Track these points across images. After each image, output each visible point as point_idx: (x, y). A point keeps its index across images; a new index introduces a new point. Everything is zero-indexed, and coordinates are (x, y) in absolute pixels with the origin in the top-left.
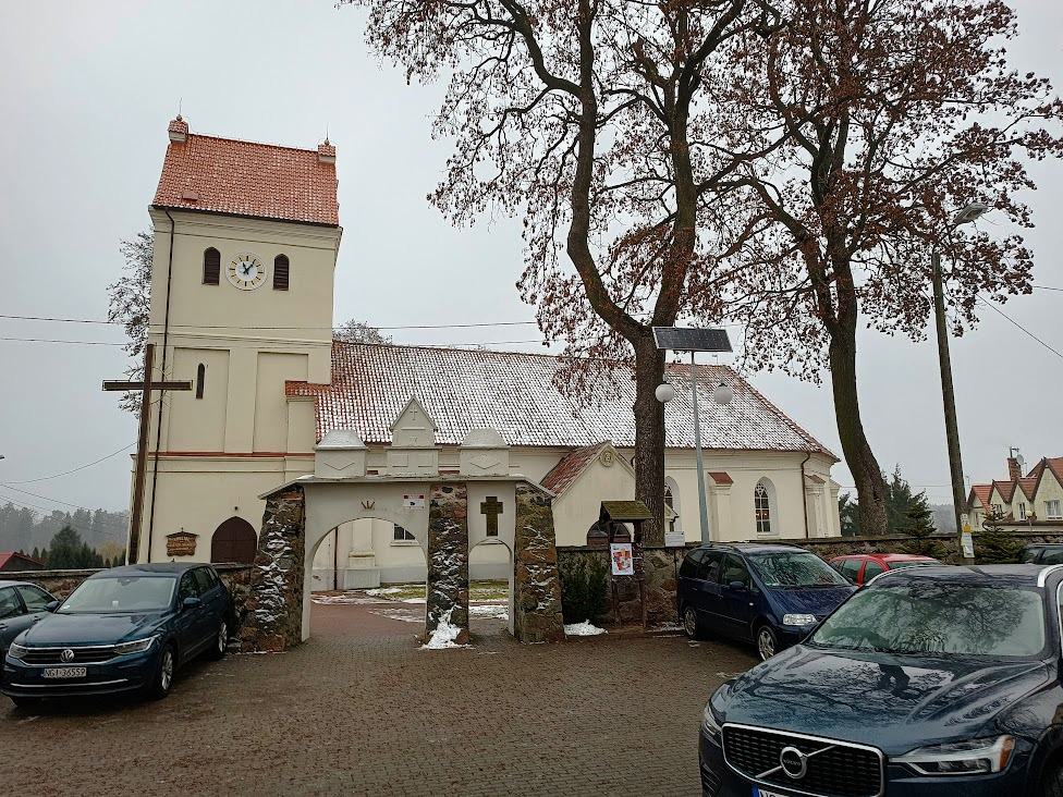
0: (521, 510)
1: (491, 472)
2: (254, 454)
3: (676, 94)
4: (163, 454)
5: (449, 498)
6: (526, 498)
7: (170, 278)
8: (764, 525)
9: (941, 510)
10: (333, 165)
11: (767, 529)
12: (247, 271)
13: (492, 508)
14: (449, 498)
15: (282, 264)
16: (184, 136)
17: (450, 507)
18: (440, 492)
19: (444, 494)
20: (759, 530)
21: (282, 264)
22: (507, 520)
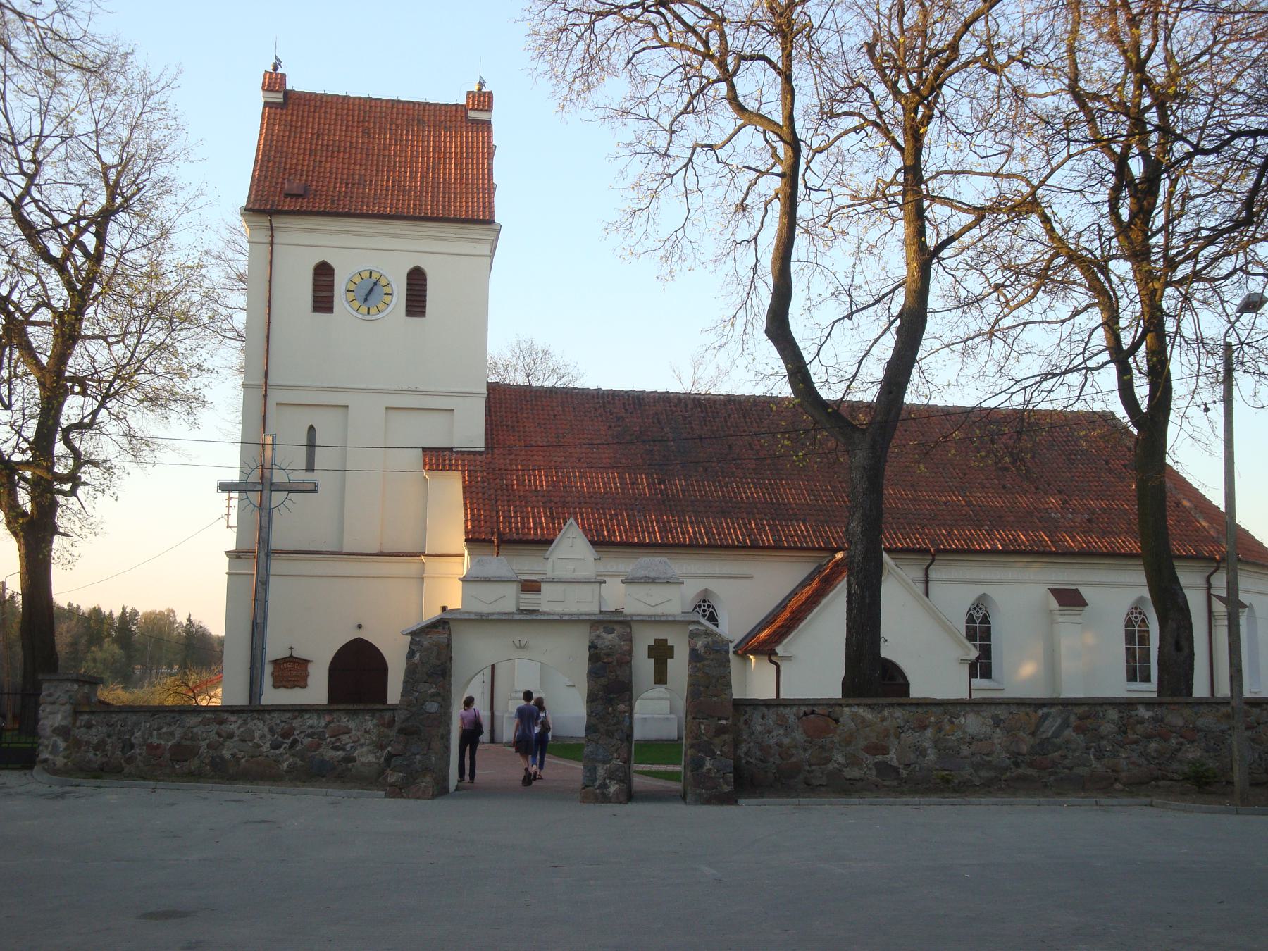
0: (695, 656)
3: (1099, 275)
5: (609, 639)
6: (700, 644)
8: (981, 668)
10: (488, 124)
11: (987, 673)
13: (661, 652)
15: (417, 280)
16: (281, 95)
17: (611, 651)
19: (604, 634)
21: (417, 280)
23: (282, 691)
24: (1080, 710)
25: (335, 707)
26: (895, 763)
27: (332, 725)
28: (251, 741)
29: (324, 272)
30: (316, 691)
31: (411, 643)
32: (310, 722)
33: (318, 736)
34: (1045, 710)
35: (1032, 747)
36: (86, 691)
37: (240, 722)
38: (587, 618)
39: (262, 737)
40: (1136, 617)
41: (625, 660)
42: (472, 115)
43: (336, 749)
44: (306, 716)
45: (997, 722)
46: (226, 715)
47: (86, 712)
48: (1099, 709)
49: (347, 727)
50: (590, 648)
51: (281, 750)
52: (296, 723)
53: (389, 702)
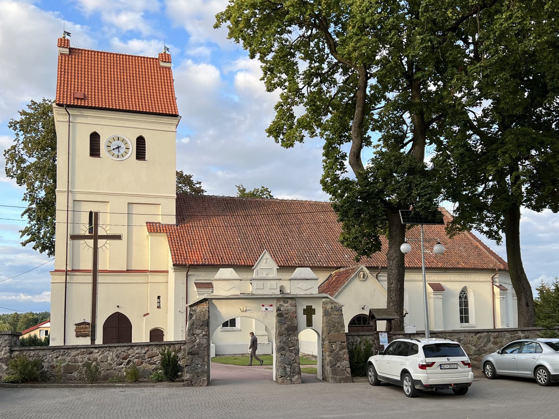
0: (326, 313)
1: (308, 292)
2: (128, 271)
4: (69, 271)
5: (286, 306)
6: (329, 306)
7: (311, 279)
8: (464, 317)
9: (309, 358)
12: (118, 147)
13: (309, 312)
14: (286, 306)
15: (141, 141)
16: (68, 50)
18: (281, 303)
20: (462, 321)
21: (141, 141)
22: (318, 318)
23: (81, 338)
25: (106, 345)
27: (149, 352)
29: (95, 138)
32: (137, 351)
33: (141, 357)
34: (479, 335)
35: (475, 351)
36: (15, 340)
37: (100, 352)
38: (276, 296)
40: (463, 295)
41: (295, 316)
42: (162, 64)
43: (152, 364)
44: (135, 348)
46: (92, 350)
47: (16, 350)
48: (502, 333)
50: (277, 311)
51: (122, 366)
52: (130, 352)
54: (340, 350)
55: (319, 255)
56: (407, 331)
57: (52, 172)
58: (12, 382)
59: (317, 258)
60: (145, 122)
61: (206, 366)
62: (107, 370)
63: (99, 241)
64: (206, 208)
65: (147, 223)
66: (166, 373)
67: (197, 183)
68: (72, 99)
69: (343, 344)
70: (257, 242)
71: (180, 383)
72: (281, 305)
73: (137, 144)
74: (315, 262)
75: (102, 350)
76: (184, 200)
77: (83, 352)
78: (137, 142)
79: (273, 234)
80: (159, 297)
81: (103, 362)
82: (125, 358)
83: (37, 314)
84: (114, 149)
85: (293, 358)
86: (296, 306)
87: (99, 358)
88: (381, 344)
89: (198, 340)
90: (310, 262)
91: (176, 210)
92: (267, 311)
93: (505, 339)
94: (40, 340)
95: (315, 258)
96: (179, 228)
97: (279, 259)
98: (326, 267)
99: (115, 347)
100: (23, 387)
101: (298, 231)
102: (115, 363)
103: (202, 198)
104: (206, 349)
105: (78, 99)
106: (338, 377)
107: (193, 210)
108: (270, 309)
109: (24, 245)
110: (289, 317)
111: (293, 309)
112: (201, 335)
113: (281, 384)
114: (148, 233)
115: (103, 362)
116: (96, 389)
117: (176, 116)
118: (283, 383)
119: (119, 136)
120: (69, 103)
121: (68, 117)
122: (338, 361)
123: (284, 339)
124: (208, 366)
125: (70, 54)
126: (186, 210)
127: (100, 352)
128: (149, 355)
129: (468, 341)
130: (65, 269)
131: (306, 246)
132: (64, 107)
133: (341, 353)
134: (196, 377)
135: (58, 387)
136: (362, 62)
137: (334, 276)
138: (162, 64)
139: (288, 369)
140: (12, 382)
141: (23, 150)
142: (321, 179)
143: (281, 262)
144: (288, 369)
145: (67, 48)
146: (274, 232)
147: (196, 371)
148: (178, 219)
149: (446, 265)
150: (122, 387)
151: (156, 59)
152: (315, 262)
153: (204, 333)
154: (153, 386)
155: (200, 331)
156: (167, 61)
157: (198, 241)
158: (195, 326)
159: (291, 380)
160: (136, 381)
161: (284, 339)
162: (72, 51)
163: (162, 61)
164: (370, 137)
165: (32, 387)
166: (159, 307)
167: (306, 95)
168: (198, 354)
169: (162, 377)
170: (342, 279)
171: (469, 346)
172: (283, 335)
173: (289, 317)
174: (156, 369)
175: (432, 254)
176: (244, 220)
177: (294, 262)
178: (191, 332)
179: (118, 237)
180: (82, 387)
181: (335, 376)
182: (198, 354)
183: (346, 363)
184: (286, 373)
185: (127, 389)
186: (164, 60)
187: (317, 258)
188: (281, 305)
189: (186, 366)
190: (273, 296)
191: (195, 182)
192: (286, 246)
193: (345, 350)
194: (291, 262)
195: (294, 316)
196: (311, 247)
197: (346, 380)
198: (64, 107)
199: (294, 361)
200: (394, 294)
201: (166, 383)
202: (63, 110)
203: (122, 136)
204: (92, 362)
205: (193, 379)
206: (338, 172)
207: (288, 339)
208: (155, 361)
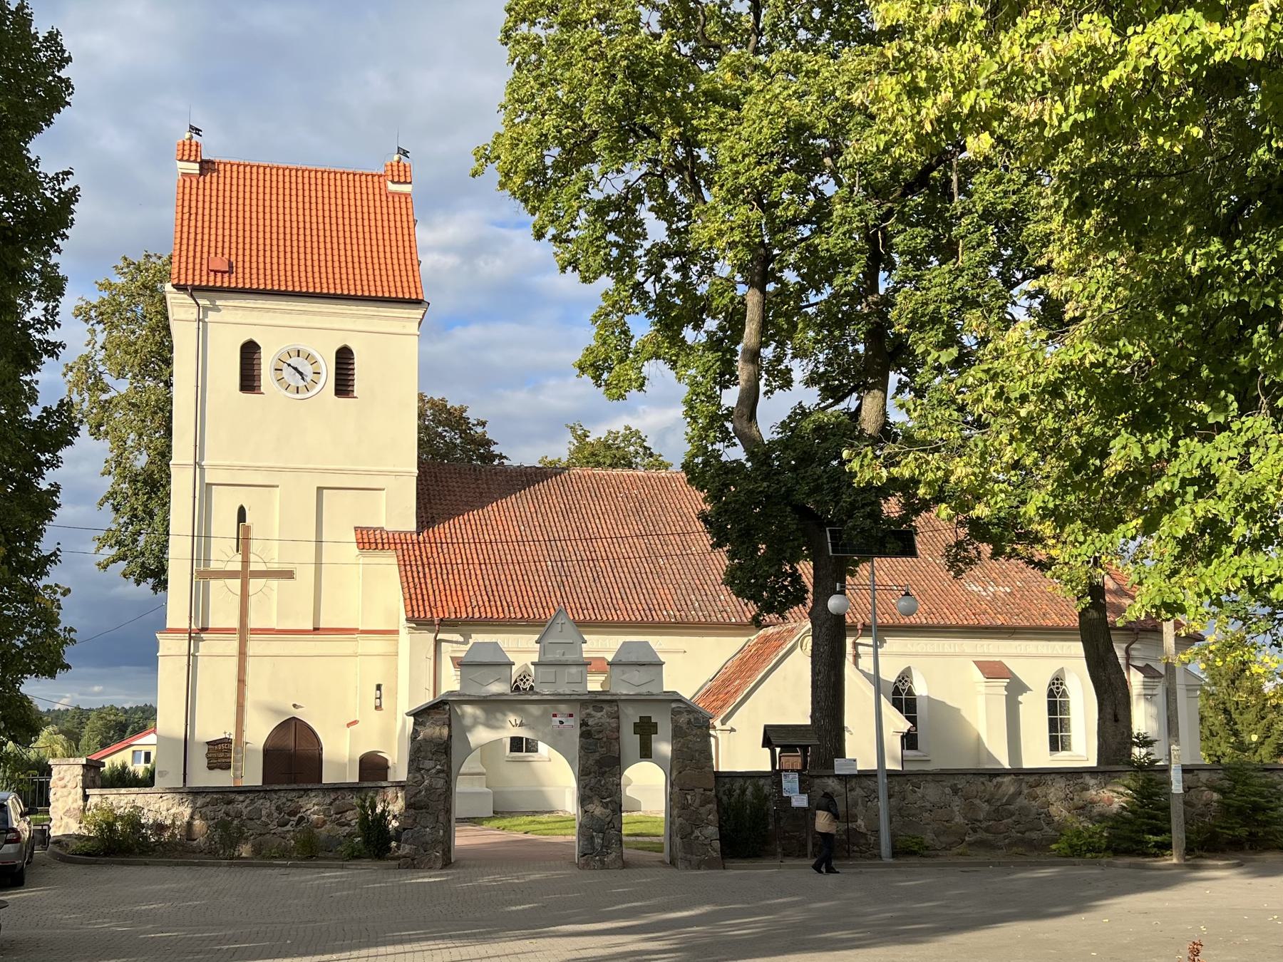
1: (644, 690)
5: (598, 717)
6: (683, 719)
15: (344, 357)
16: (197, 166)
18: (590, 710)
21: (344, 357)
23: (217, 772)
24: (1031, 779)
25: (366, 784)
26: (863, 830)
27: (337, 802)
28: (259, 819)
29: (250, 351)
30: (253, 775)
31: (415, 724)
35: (988, 813)
37: (248, 801)
39: (269, 816)
40: (1058, 688)
42: (392, 187)
45: (955, 791)
46: (232, 796)
49: (352, 804)
50: (581, 725)
51: (288, 827)
53: (324, 781)
54: (702, 806)
55: (722, 597)
56: (841, 770)
57: (163, 411)
58: (87, 854)
59: (719, 603)
60: (353, 316)
61: (441, 832)
62: (260, 835)
63: (252, 581)
64: (481, 493)
65: (356, 529)
66: (367, 842)
67: (478, 424)
68: (204, 273)
69: (708, 793)
70: (588, 568)
71: (393, 863)
72: (589, 715)
73: (337, 363)
74: (713, 614)
75: (251, 796)
76: (436, 477)
77: (217, 799)
78: (337, 358)
79: (624, 551)
80: (379, 687)
81: (252, 819)
82: (291, 814)
83: (126, 711)
84: (289, 365)
85: (608, 819)
86: (618, 718)
87: (245, 812)
88: (785, 795)
89: (426, 782)
90: (700, 614)
91: (417, 494)
92: (561, 726)
93: (1053, 789)
94: (134, 774)
95: (713, 603)
96: (421, 537)
97: (634, 606)
98: (736, 624)
99: (276, 791)
100: (106, 863)
101: (680, 543)
102: (275, 823)
103: (475, 470)
104: (442, 797)
105: (216, 272)
106: (695, 857)
107: (454, 498)
108: (569, 722)
109: (105, 568)
110: (605, 739)
111: (613, 722)
112: (434, 771)
113: (583, 868)
114: (357, 552)
115: (252, 819)
116: (237, 869)
117: (418, 302)
118: (586, 866)
119: (299, 347)
120: (197, 283)
121: (196, 310)
122: (698, 826)
123: (593, 780)
124: (444, 832)
125: (200, 175)
126: (440, 499)
127: (248, 801)
128: (338, 807)
129: (975, 793)
130: (187, 627)
131: (695, 577)
132: (187, 290)
133: (702, 810)
134: (422, 851)
135: (169, 864)
136: (736, 256)
137: (754, 645)
138: (392, 187)
139: (598, 841)
140: (87, 854)
141: (104, 364)
142: (683, 461)
143: (637, 613)
144: (598, 841)
145: (195, 161)
146: (627, 546)
147: (423, 840)
148: (420, 520)
149: (1016, 621)
150: (285, 866)
151: (380, 176)
152: (713, 614)
153: (438, 767)
154: (342, 867)
155: (431, 764)
156: (402, 179)
157: (460, 566)
158: (423, 754)
159: (602, 861)
160: (311, 857)
161: (593, 780)
162: (206, 166)
163: (393, 182)
164: (791, 370)
165: (123, 864)
166: (378, 708)
167: (652, 294)
168: (426, 807)
169: (359, 851)
170: (768, 651)
171: (977, 801)
172: (590, 773)
173: (605, 739)
174: (349, 835)
175: (984, 594)
176: (561, 518)
177: (665, 613)
178: (415, 764)
179: (289, 575)
180: (213, 865)
181: (689, 856)
182: (426, 807)
183: (712, 830)
184: (593, 848)
185: (294, 870)
186: (396, 179)
187: (719, 603)
188: (589, 715)
189: (404, 829)
190: (573, 697)
191: (473, 421)
192: (650, 576)
193: (711, 806)
194: (659, 612)
195: (614, 736)
196: (707, 578)
197: (710, 864)
198: (187, 290)
199: (611, 825)
200: (823, 694)
201: (365, 863)
202: (184, 298)
203: (306, 347)
204: (233, 820)
205: (416, 854)
206: (718, 446)
207: (600, 781)
208: (349, 818)
